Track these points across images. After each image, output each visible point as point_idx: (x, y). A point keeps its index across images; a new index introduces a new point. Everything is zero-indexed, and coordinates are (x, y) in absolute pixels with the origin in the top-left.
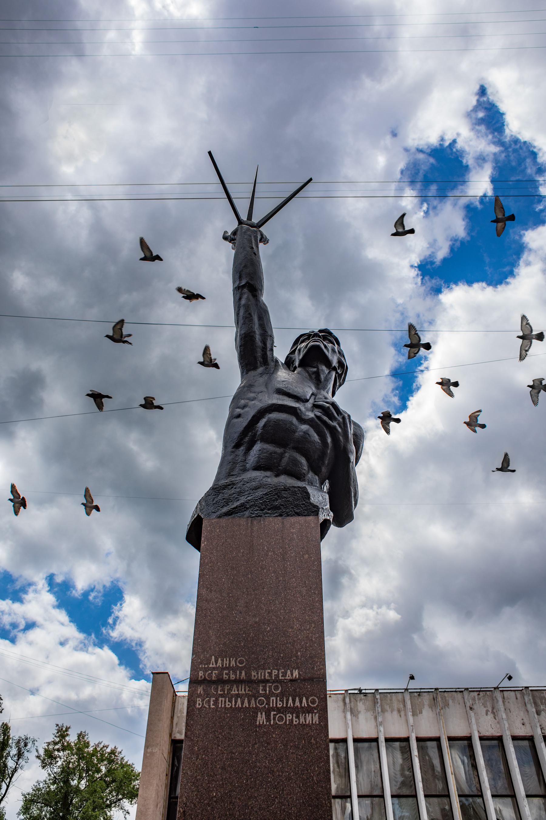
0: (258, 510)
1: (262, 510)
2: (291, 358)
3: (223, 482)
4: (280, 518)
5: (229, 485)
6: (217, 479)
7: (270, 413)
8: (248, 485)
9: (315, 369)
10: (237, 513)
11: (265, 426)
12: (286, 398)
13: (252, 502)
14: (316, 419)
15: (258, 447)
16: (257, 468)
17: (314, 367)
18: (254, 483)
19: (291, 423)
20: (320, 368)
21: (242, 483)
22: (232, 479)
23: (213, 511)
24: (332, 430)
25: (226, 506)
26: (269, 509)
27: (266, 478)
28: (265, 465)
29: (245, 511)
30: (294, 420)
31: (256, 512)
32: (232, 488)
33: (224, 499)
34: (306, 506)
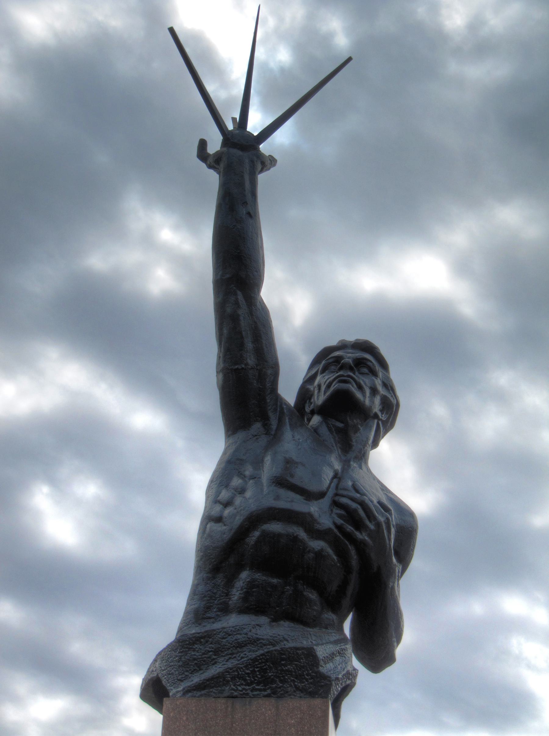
0: (242, 684)
1: (248, 685)
2: (308, 390)
3: (194, 630)
4: (273, 700)
5: (202, 638)
6: (185, 624)
7: (265, 523)
8: (229, 638)
9: (340, 425)
10: (213, 688)
11: (258, 541)
12: (291, 495)
13: (234, 671)
14: (336, 530)
15: (245, 575)
16: (243, 611)
17: (342, 422)
18: (239, 636)
19: (295, 539)
20: (350, 422)
21: (222, 634)
22: (209, 626)
23: (180, 677)
24: (360, 546)
25: (197, 671)
26: (258, 684)
27: (258, 628)
28: (255, 605)
29: (224, 685)
30: (302, 534)
31: (240, 688)
32: (207, 642)
33: (195, 659)
34: (312, 678)
